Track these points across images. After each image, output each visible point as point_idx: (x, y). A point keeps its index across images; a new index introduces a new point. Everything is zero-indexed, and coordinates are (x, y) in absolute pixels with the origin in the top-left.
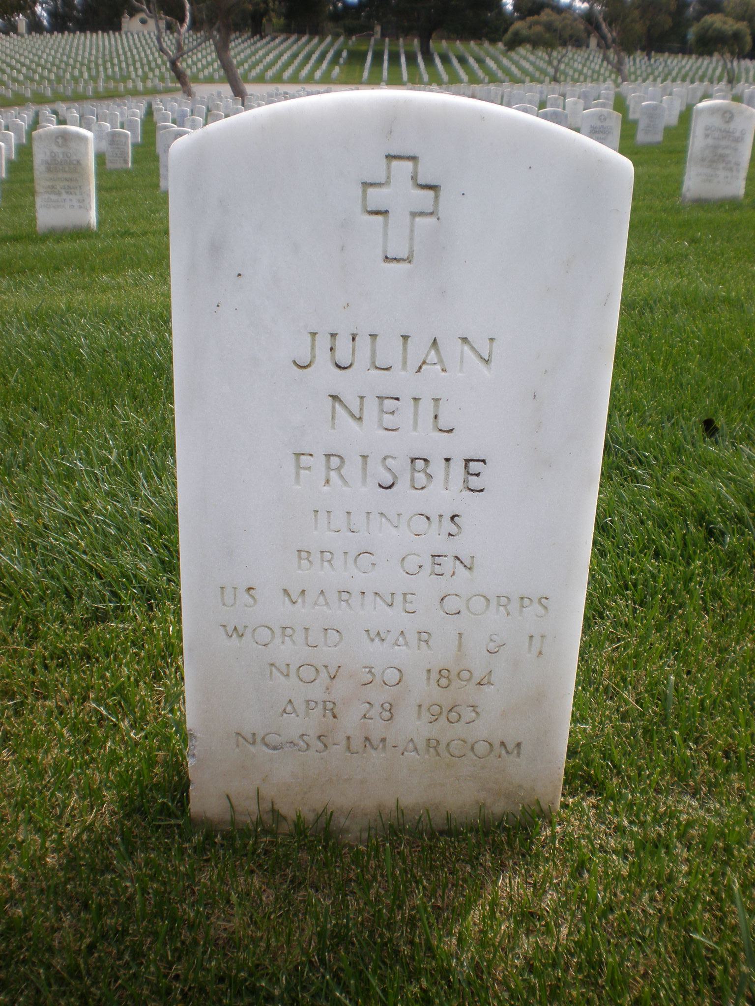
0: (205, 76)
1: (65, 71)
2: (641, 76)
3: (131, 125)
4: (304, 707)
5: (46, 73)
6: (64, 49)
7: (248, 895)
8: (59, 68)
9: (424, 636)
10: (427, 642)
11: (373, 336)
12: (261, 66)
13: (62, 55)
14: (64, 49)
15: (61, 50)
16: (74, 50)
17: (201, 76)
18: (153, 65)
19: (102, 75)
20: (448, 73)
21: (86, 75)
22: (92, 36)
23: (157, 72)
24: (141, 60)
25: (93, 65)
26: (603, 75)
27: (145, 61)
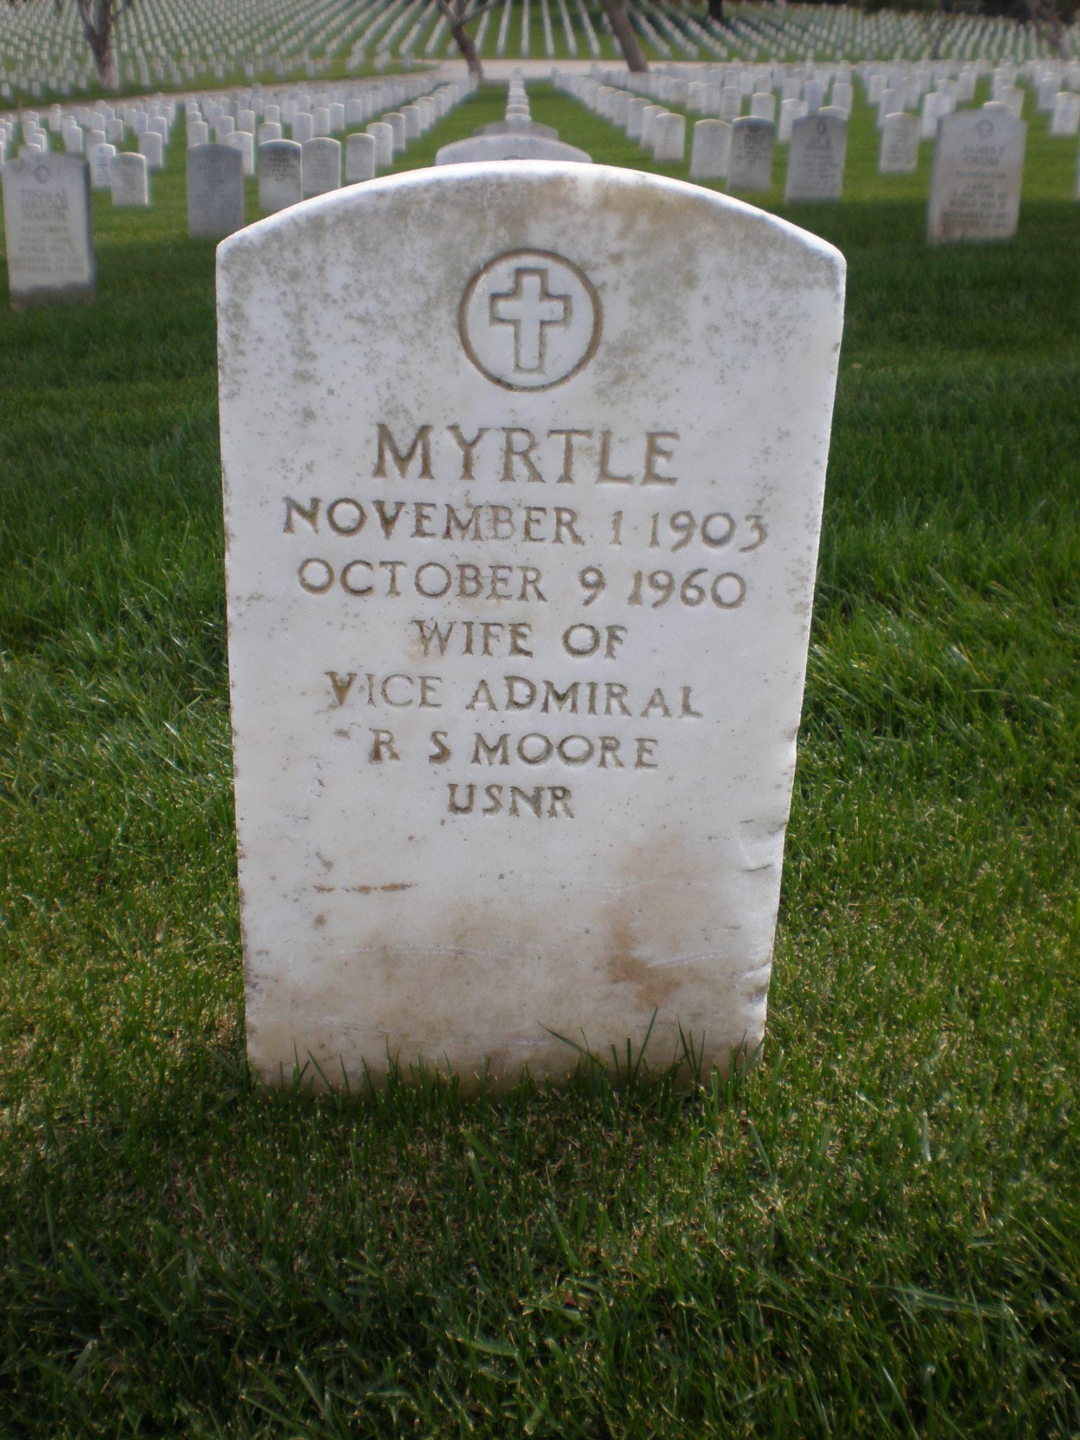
1: (40, 49)
5: (34, 51)
12: (301, 35)
16: (152, 21)
18: (146, 36)
22: (1006, 30)
23: (195, 46)
24: (170, 29)
27: (70, 33)
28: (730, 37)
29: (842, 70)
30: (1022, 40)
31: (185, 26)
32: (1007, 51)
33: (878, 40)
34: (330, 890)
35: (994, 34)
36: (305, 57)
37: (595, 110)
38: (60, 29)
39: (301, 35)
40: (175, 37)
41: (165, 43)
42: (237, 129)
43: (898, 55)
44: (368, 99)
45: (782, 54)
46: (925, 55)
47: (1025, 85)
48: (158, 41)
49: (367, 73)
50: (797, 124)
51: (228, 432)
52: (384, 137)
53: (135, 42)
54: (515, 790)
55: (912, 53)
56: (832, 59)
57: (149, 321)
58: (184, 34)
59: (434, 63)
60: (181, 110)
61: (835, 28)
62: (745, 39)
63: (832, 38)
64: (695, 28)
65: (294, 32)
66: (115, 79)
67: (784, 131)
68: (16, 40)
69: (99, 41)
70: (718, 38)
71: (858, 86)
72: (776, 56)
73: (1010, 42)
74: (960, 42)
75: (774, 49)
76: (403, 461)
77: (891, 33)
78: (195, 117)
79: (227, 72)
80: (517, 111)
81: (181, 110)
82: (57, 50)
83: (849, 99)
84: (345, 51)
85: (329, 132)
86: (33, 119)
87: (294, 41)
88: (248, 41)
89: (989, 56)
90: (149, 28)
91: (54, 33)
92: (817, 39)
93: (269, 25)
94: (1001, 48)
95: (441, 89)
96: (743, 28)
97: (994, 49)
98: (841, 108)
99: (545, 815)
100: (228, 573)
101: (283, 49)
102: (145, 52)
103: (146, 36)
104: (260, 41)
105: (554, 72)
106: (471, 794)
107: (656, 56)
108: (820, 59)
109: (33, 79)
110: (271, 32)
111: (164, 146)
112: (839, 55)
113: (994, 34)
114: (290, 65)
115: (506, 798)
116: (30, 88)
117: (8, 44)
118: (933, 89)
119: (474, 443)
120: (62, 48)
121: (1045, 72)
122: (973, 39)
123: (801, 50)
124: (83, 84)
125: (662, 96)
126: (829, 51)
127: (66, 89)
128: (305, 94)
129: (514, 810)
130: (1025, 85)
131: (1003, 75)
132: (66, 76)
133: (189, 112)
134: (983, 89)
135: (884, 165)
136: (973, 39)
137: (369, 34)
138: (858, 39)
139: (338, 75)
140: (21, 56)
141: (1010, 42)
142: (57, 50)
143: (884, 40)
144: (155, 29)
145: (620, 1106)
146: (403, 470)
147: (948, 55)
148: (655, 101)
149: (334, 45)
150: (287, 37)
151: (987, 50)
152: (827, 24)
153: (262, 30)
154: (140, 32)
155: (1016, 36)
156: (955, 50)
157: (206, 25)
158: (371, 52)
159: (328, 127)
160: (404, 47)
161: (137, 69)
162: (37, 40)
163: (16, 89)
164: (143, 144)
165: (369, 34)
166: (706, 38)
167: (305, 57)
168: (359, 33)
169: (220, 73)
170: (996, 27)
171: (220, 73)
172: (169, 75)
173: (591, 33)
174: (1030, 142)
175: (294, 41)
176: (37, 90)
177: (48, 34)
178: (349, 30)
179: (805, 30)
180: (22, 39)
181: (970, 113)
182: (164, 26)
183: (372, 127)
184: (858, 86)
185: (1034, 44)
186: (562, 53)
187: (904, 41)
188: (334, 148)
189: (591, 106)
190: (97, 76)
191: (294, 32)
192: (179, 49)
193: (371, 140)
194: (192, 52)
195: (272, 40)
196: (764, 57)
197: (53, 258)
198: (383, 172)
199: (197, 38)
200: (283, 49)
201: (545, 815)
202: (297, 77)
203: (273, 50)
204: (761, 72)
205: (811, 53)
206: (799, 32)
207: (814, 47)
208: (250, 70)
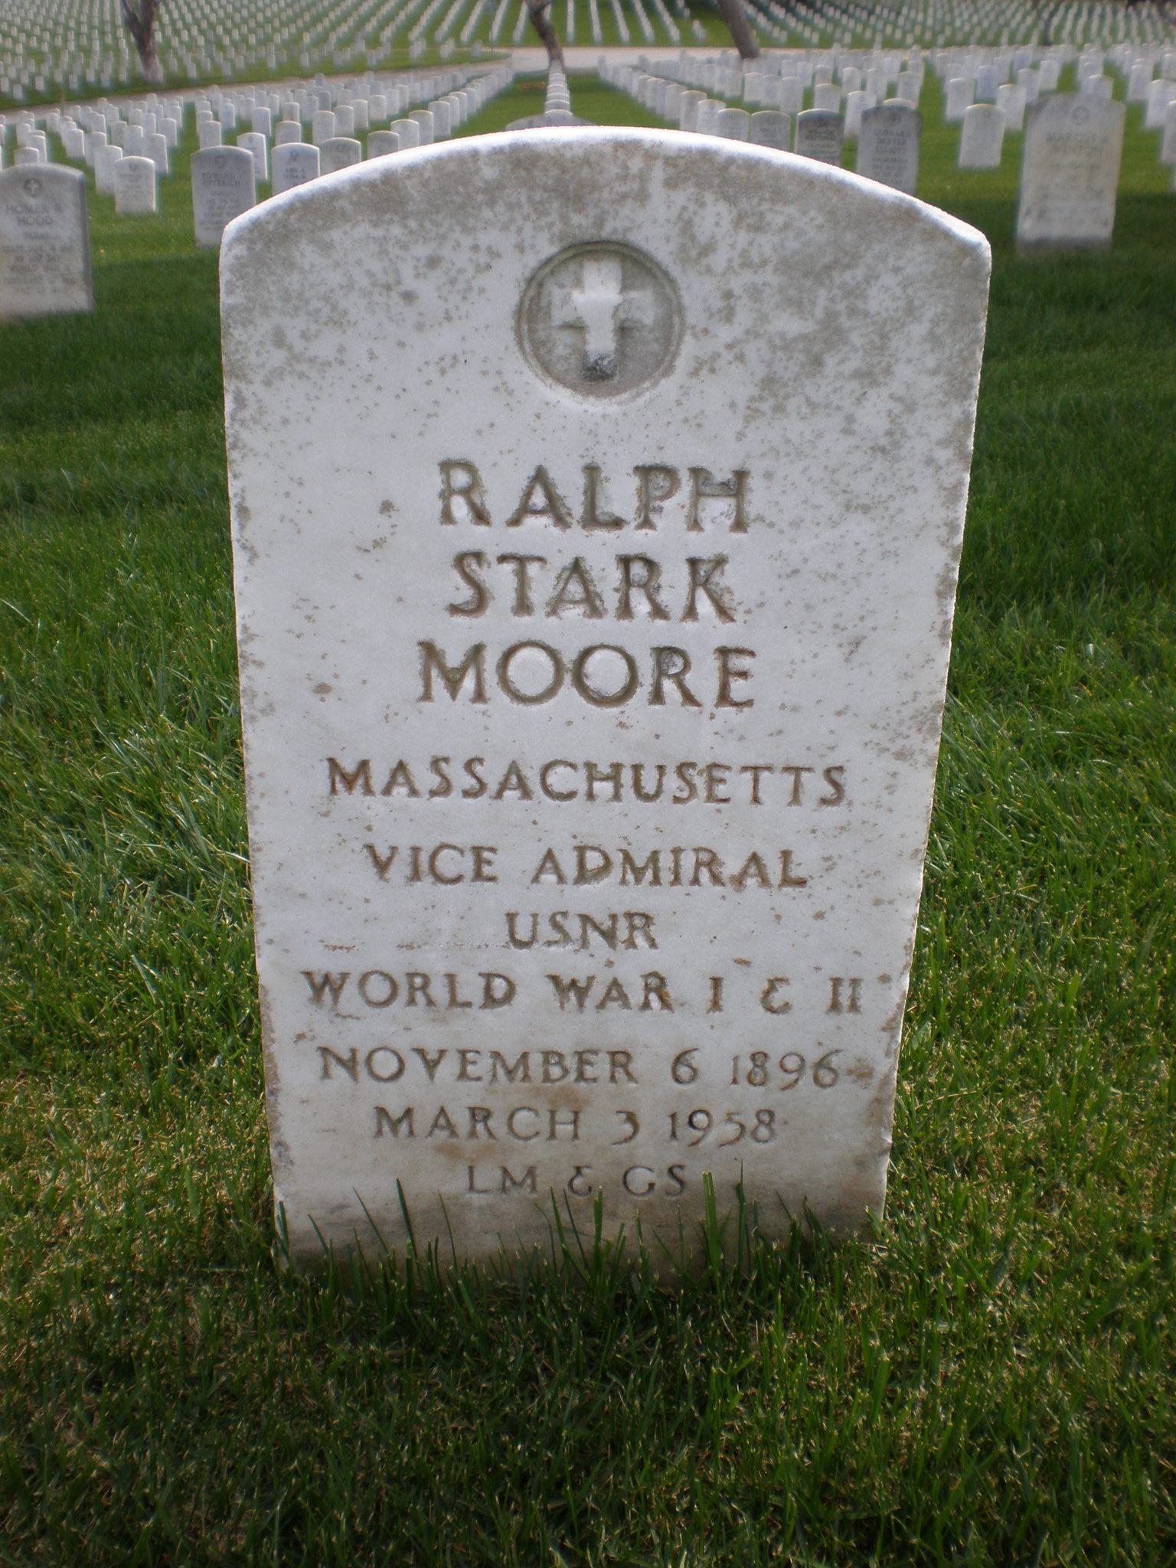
0: (283, 40)
3: (164, 128)
4: (616, 575)
6: (48, 10)
7: (27, 766)
8: (29, 35)
9: (621, 1058)
10: (625, 1067)
11: (735, 1081)
12: (351, 22)
13: (46, 18)
14: (48, 10)
15: (43, 11)
18: (180, 24)
19: (97, 46)
20: (603, 27)
21: (97, 46)
22: (1115, 12)
25: (108, 28)
26: (961, 28)
27: (96, 22)
28: (819, 21)
29: (914, 56)
30: (1134, 24)
31: (198, 14)
32: (1121, 36)
33: (980, 23)
34: (400, 947)
35: (1103, 16)
36: (361, 46)
38: (84, 18)
39: (351, 22)
40: (187, 27)
41: (201, 32)
43: (1004, 39)
45: (848, 38)
46: (1035, 38)
47: (1111, 70)
48: (195, 31)
50: (867, 116)
53: (169, 31)
54: (585, 919)
55: (1019, 36)
56: (901, 45)
58: (197, 22)
59: (503, 51)
60: (190, 113)
61: (931, 11)
62: (837, 24)
63: (930, 22)
64: (778, 11)
65: (343, 18)
66: (160, 73)
67: (852, 120)
68: (14, 32)
69: (141, 27)
70: (807, 23)
72: (840, 41)
73: (1122, 26)
74: (1069, 25)
75: (807, 33)
77: (939, 15)
78: (207, 117)
79: (279, 63)
80: (559, 106)
81: (190, 113)
82: (59, 42)
84: (401, 40)
86: (28, 123)
87: (344, 29)
88: (293, 30)
89: (1073, 41)
90: (182, 17)
91: (79, 23)
92: (914, 23)
93: (314, 11)
94: (1114, 31)
95: (474, 82)
96: (830, 12)
97: (1106, 32)
98: (908, 99)
99: (621, 946)
103: (180, 24)
104: (307, 29)
105: (602, 61)
106: (535, 924)
107: (776, 45)
108: (889, 44)
109: (67, 70)
110: (317, 20)
112: (909, 39)
113: (1103, 16)
115: (574, 927)
116: (67, 81)
117: (6, 35)
120: (90, 39)
121: (1133, 59)
122: (1082, 21)
123: (868, 34)
124: (124, 77)
125: (717, 88)
126: (898, 35)
127: (106, 82)
129: (585, 942)
130: (1111, 70)
131: (1090, 60)
132: (99, 69)
133: (199, 111)
134: (1068, 80)
135: (964, 158)
136: (1082, 21)
137: (424, 20)
138: (958, 23)
139: (400, 65)
140: (46, 48)
141: (1122, 26)
142: (84, 41)
144: (189, 18)
147: (1058, 40)
148: (711, 95)
149: (388, 33)
150: (334, 27)
151: (1072, 34)
152: (921, 6)
153: (307, 17)
154: (173, 22)
155: (1127, 17)
156: (1065, 34)
157: (221, 13)
159: (352, 127)
160: (466, 34)
161: (180, 60)
162: (37, 30)
163: (51, 83)
164: (255, 123)
165: (424, 20)
166: (792, 22)
167: (361, 46)
168: (413, 20)
169: (272, 64)
170: (1104, 9)
171: (272, 64)
173: (667, 18)
174: (1127, 135)
175: (344, 29)
176: (74, 83)
177: (72, 24)
178: (402, 16)
179: (898, 13)
180: (21, 30)
181: (1083, 112)
182: (198, 14)
185: (1148, 26)
186: (611, 39)
187: (952, 23)
190: (140, 68)
191: (343, 18)
194: (207, 41)
195: (320, 28)
196: (826, 43)
199: (187, 27)
201: (621, 946)
202: (357, 68)
203: (323, 39)
204: (823, 61)
205: (879, 38)
206: (838, 14)
207: (883, 31)
208: (305, 61)
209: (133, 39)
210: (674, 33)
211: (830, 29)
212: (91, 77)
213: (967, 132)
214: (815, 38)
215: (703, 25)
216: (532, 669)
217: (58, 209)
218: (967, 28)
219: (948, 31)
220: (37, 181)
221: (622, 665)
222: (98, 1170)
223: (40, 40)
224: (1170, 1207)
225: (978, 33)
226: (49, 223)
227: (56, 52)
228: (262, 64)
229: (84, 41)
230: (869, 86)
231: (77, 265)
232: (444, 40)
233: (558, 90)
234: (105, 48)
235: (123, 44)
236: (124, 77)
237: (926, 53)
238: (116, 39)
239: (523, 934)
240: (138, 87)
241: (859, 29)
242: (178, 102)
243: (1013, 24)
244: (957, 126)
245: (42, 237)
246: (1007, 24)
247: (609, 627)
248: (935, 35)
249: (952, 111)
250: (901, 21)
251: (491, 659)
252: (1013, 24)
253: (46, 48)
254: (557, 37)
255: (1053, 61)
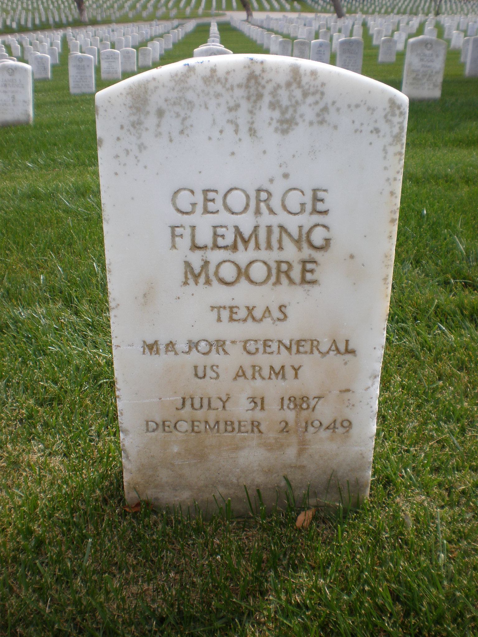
2: (378, 6)
17: (144, 14)
19: (20, 7)
21: (20, 7)
33: (386, 4)
37: (249, 36)
42: (91, 45)
44: (159, 27)
49: (150, 19)
51: (101, 164)
52: (156, 49)
55: (414, 10)
57: (63, 131)
71: (364, 24)
76: (196, 277)
83: (361, 31)
85: (131, 45)
98: (357, 36)
100: (105, 215)
101: (105, 6)
102: (43, 7)
111: (59, 53)
114: (118, 15)
118: (398, 29)
119: (299, 369)
120: (17, 5)
128: (122, 28)
136: (448, 5)
139: (138, 18)
140: (9, 8)
142: (14, 6)
143: (388, 4)
145: (286, 520)
146: (197, 283)
151: (423, 9)
158: (156, 7)
169: (131, 15)
172: (47, 20)
183: (149, 44)
184: (364, 24)
187: (374, 3)
188: (133, 52)
189: (248, 34)
192: (48, 5)
193: (149, 50)
197: (20, 105)
198: (156, 65)
200: (105, 6)
209: (76, 4)
210: (288, 6)
211: (325, 5)
212: (57, 19)
213: (381, 51)
214: (320, 8)
215: (298, 3)
216: (228, 272)
217: (437, 56)
218: (404, 7)
219: (397, 8)
220: (431, 44)
221: (265, 268)
222: (46, 468)
223: (7, 5)
224: (2, 542)
225: (409, 8)
226: (432, 61)
227: (14, 10)
228: (126, 15)
229: (14, 6)
230: (342, 31)
231: (439, 79)
232: (162, 6)
233: (214, 29)
234: (23, 8)
235: (72, 6)
236: (70, 19)
237: (364, 16)
238: (38, 5)
239: (201, 374)
240: (78, 24)
241: (349, 6)
242: (58, 36)
243: (400, 5)
244: (377, 47)
245: (429, 67)
246: (397, 4)
247: (263, 254)
248: (380, 9)
249: (375, 42)
250: (377, 3)
251: (212, 269)
252: (400, 5)
253: (9, 8)
254: (250, 7)
255: (415, 22)
